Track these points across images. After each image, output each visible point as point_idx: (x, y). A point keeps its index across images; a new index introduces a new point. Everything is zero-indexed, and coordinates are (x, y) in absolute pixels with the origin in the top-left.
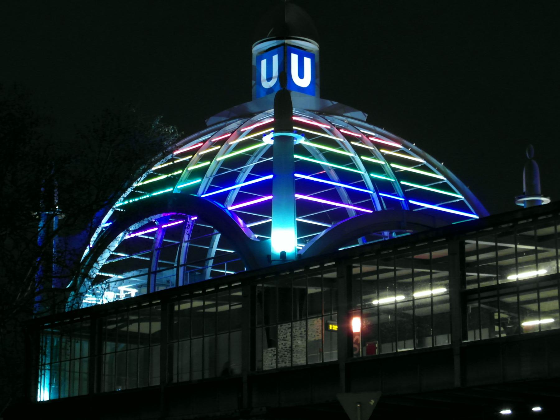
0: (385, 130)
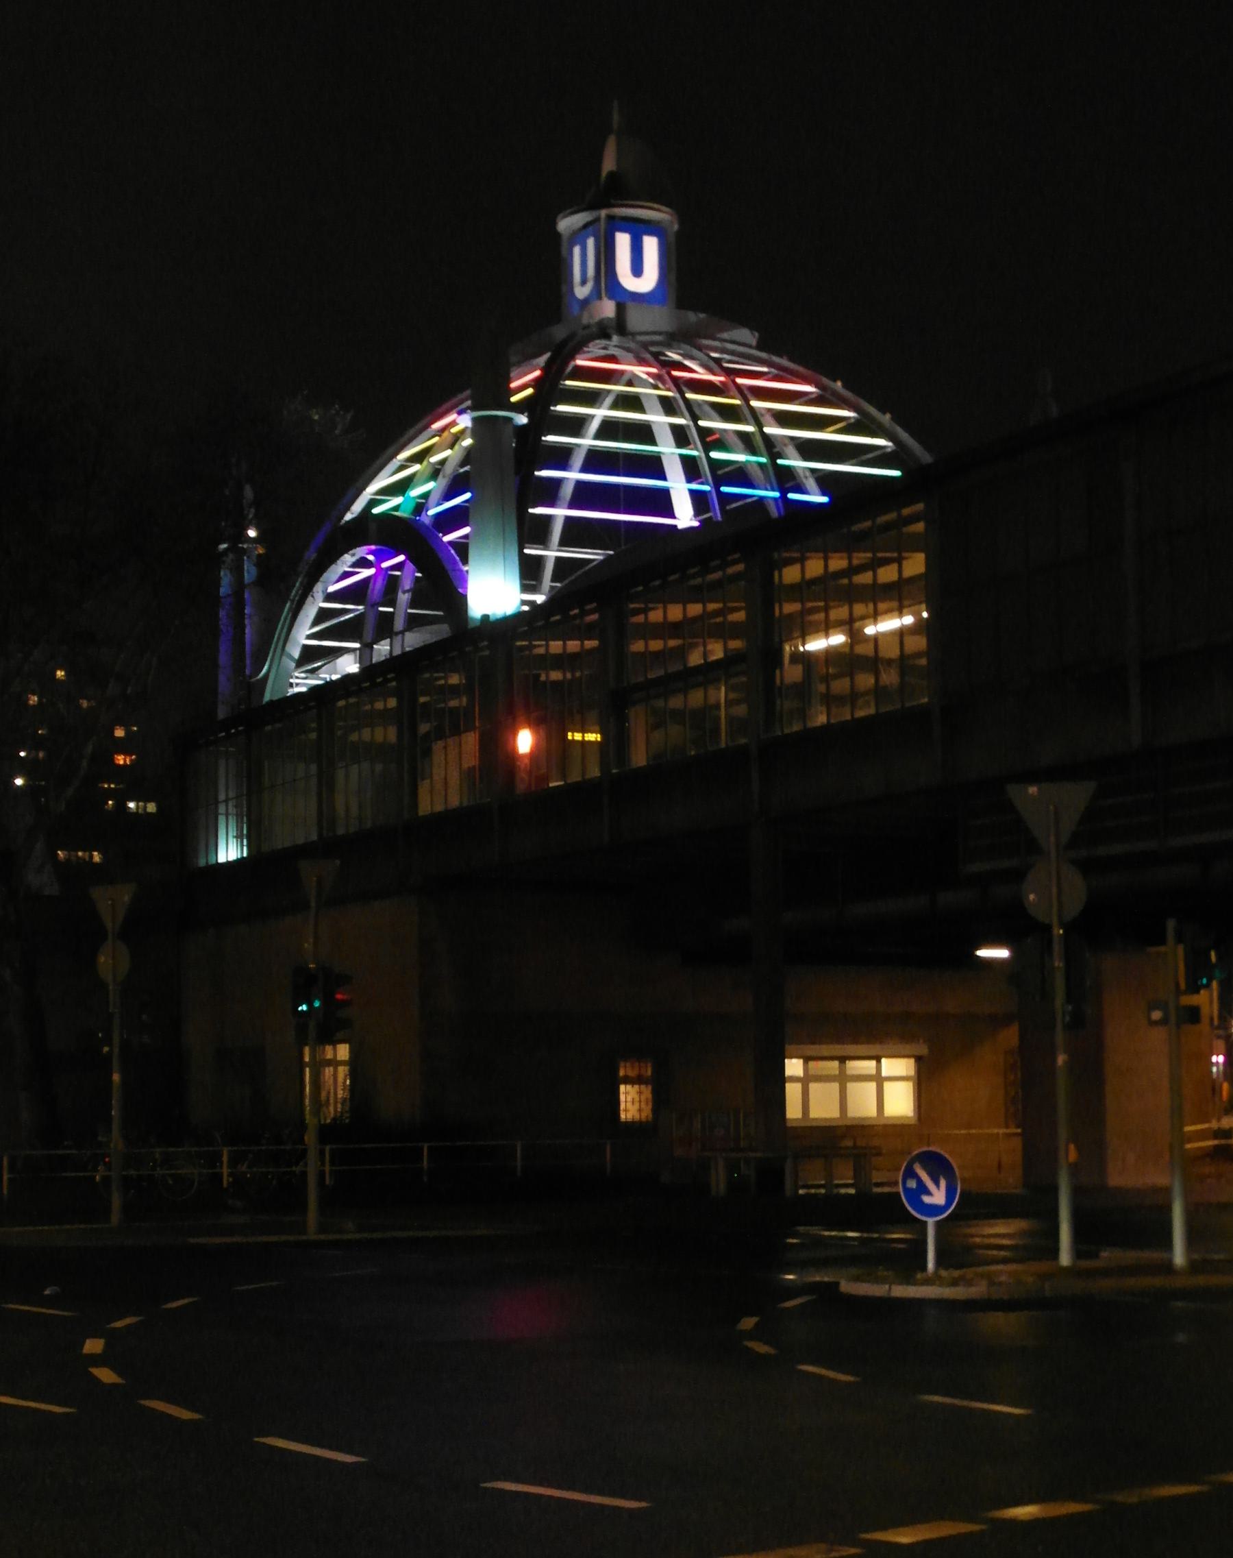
0: (791, 359)
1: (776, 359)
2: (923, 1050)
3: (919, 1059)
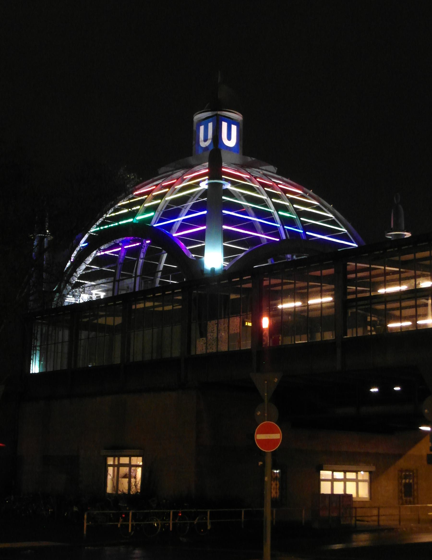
0: (290, 179)
1: (285, 179)
2: (373, 469)
3: (370, 473)
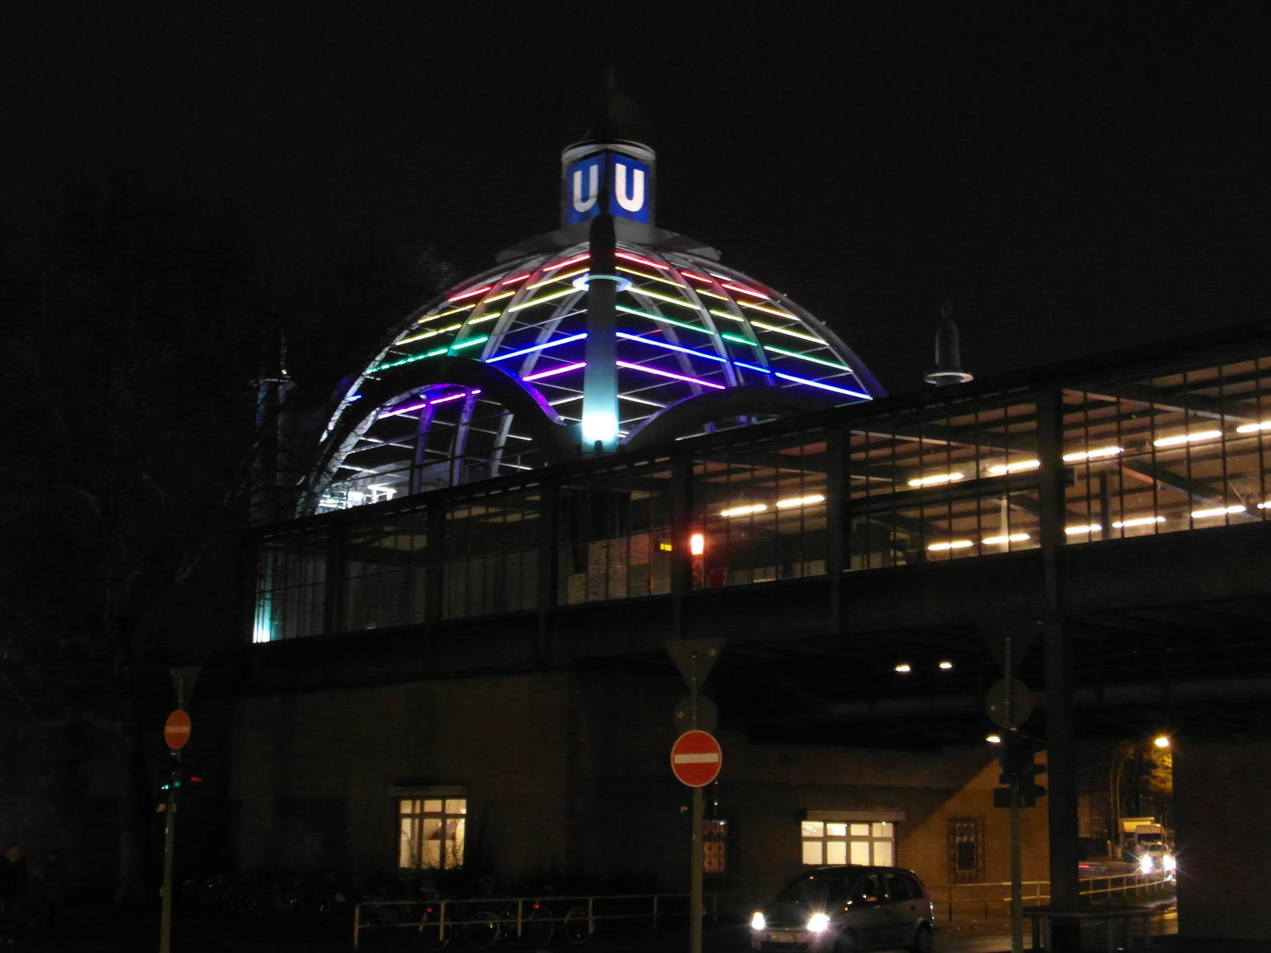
0: (746, 274)
2: (901, 816)
3: (896, 824)
